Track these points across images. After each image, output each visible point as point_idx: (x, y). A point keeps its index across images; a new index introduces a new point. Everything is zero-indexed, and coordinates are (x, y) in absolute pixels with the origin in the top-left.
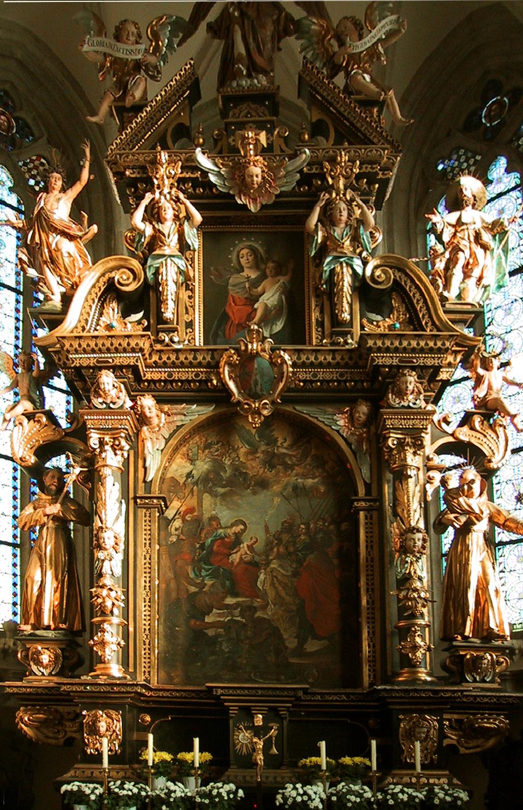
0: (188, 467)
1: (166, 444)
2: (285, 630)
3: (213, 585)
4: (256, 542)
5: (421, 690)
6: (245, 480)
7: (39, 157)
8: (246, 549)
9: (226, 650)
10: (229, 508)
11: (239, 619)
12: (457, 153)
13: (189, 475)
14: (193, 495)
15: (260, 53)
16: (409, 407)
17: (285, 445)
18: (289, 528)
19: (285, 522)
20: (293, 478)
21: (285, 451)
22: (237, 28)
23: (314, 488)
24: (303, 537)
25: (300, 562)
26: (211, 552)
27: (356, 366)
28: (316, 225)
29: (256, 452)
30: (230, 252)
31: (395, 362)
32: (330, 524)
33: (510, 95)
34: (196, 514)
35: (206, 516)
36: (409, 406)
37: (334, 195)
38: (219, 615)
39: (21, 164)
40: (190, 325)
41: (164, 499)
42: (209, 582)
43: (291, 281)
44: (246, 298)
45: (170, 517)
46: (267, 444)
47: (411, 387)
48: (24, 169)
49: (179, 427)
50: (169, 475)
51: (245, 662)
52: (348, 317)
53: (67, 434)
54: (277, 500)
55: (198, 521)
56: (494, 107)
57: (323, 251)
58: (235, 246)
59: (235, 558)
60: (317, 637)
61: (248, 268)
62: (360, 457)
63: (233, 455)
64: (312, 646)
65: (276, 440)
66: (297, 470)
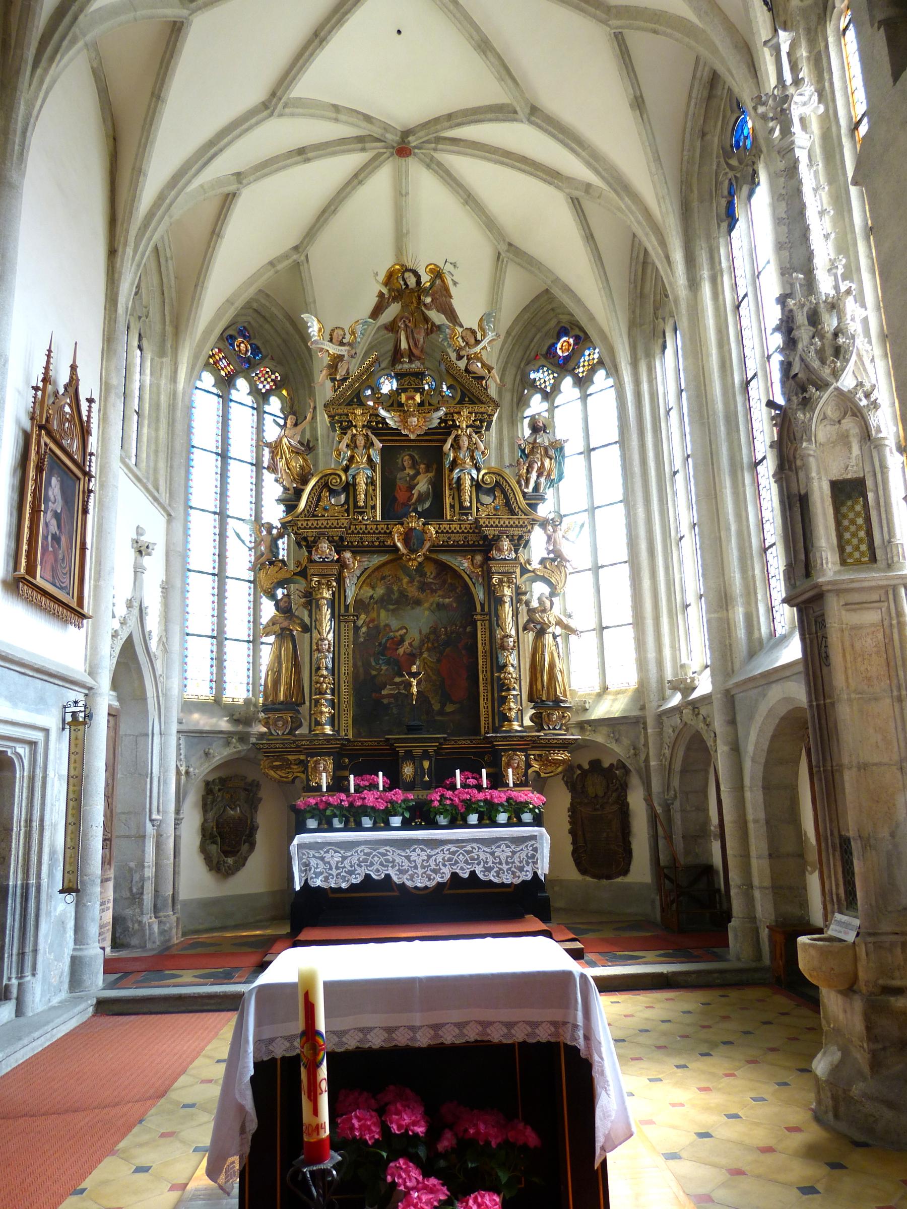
0: (371, 592)
7: (265, 367)
13: (372, 597)
16: (505, 559)
18: (434, 630)
20: (437, 598)
22: (403, 333)
26: (385, 648)
27: (474, 532)
31: (496, 533)
35: (382, 624)
38: (391, 689)
41: (357, 616)
42: (384, 668)
43: (435, 477)
47: (506, 548)
49: (366, 569)
50: (359, 598)
53: (295, 574)
54: (427, 613)
55: (377, 627)
57: (454, 464)
58: (400, 454)
59: (401, 651)
60: (452, 702)
64: (449, 708)
65: (426, 574)
66: (440, 593)
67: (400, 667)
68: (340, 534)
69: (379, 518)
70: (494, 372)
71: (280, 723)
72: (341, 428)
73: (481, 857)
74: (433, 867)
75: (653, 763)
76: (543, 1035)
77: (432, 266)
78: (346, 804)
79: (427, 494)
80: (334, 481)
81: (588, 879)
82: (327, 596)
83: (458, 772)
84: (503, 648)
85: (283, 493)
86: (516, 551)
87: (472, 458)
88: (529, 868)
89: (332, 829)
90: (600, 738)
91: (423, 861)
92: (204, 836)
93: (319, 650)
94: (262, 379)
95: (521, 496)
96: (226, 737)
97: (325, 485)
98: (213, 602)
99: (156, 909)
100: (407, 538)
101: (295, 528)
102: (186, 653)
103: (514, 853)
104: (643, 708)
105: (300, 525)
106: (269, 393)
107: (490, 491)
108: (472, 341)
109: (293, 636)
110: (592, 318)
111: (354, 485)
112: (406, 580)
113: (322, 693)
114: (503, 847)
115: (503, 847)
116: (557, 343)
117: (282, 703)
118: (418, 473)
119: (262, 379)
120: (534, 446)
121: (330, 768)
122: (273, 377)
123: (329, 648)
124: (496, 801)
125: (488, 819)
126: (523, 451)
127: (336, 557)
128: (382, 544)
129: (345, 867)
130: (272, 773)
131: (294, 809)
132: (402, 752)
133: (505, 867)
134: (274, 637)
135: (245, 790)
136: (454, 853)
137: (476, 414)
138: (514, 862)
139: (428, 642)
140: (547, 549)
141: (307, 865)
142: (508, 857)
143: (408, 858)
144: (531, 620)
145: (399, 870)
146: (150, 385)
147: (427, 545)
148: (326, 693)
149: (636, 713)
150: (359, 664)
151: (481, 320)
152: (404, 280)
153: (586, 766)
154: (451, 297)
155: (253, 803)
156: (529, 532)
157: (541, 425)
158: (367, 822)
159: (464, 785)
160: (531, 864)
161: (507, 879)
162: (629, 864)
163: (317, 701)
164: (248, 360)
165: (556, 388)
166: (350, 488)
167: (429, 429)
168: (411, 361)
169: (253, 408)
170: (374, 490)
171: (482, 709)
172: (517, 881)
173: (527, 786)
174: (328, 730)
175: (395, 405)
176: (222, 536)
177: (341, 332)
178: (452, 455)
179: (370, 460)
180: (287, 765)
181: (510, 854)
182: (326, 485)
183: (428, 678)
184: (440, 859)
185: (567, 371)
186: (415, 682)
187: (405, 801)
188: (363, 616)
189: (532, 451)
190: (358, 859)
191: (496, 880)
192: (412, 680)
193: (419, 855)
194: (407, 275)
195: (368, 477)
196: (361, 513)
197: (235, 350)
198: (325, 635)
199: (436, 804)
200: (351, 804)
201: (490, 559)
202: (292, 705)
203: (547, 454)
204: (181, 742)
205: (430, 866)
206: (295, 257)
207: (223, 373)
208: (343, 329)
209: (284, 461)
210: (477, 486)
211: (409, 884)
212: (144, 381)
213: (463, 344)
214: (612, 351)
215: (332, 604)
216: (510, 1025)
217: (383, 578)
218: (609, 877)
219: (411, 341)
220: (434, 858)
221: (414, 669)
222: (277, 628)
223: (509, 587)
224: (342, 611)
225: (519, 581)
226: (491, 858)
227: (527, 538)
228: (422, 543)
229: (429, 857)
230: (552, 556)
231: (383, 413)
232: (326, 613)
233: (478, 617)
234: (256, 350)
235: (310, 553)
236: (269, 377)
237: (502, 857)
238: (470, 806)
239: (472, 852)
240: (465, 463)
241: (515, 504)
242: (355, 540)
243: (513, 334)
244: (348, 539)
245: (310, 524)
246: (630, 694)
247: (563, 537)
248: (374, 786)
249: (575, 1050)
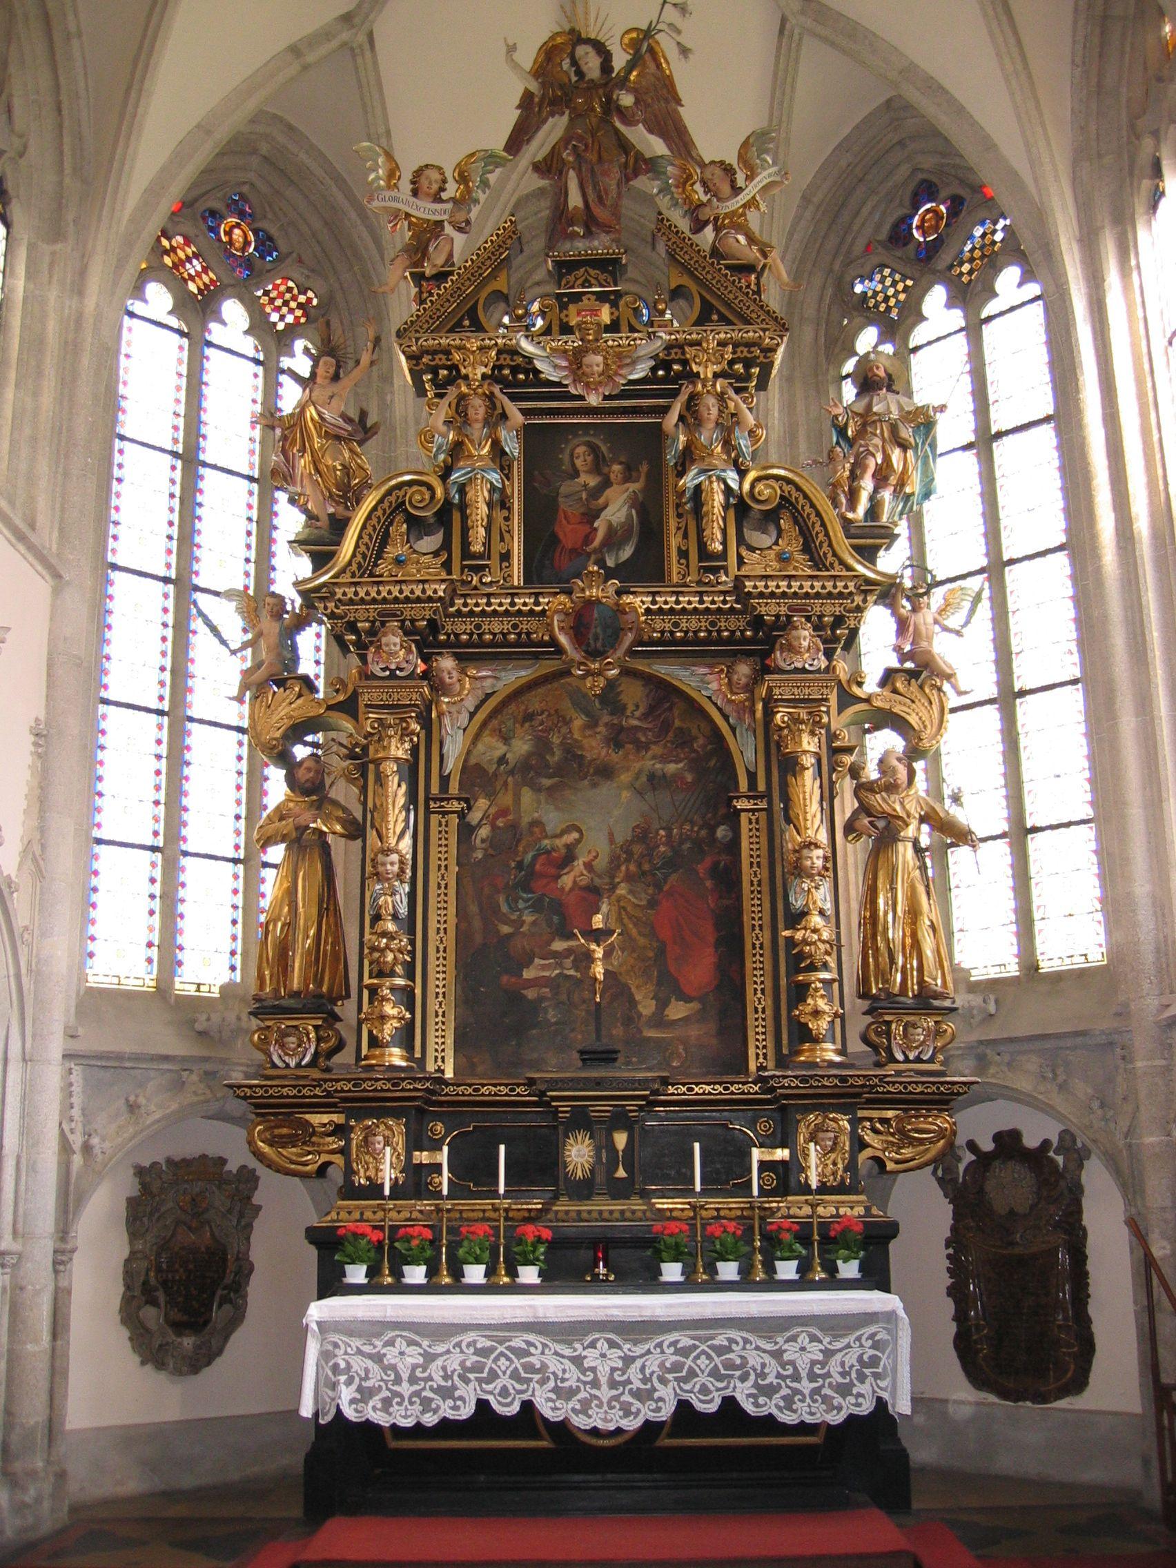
0: (500, 750)
1: (470, 720)
2: (638, 987)
3: (534, 923)
4: (596, 857)
5: (823, 1077)
6: (580, 765)
7: (285, 279)
8: (582, 867)
9: (553, 1020)
10: (557, 809)
11: (572, 972)
12: (881, 272)
13: (502, 760)
14: (507, 790)
15: (600, 200)
16: (804, 671)
17: (637, 714)
18: (642, 835)
19: (637, 826)
20: (648, 763)
21: (635, 723)
23: (677, 776)
24: (662, 849)
25: (658, 886)
26: (531, 874)
28: (676, 425)
29: (596, 725)
30: (562, 451)
31: (783, 610)
32: (701, 828)
33: (949, 202)
34: (510, 817)
35: (525, 820)
36: (804, 667)
37: (700, 387)
38: (544, 967)
39: (260, 293)
40: (506, 557)
41: (467, 801)
42: (528, 918)
43: (645, 490)
44: (583, 514)
45: (474, 823)
46: (612, 714)
48: (265, 300)
50: (473, 761)
51: (580, 1037)
52: (720, 548)
53: (330, 708)
54: (626, 794)
55: (514, 827)
56: (928, 217)
57: (687, 458)
58: (567, 442)
59: (567, 881)
61: (586, 472)
62: (742, 734)
63: (564, 730)
64: (677, 1010)
65: (624, 708)
66: (656, 750)
68: (428, 614)
69: (517, 578)
70: (775, 255)
73: (751, 1362)
74: (637, 1384)
77: (634, 35)
79: (627, 528)
80: (417, 496)
82: (400, 754)
84: (799, 871)
85: (306, 526)
86: (829, 654)
87: (727, 444)
88: (865, 1388)
91: (613, 1370)
94: (279, 302)
95: (839, 528)
98: (158, 773)
100: (579, 623)
101: (331, 605)
102: (95, 882)
103: (828, 1353)
105: (339, 596)
106: (292, 331)
107: (771, 517)
110: (989, 145)
111: (463, 507)
112: (579, 722)
114: (803, 1339)
115: (803, 1339)
116: (912, 217)
117: (296, 994)
118: (606, 483)
119: (279, 302)
120: (867, 420)
122: (302, 299)
123: (402, 871)
126: (842, 432)
127: (421, 667)
128: (526, 641)
129: (430, 1378)
132: (564, 1108)
133: (806, 1386)
134: (282, 846)
136: (685, 1352)
137: (735, 346)
138: (828, 1375)
139: (628, 860)
140: (898, 649)
142: (813, 1363)
144: (864, 809)
145: (555, 1389)
146: (25, 299)
148: (392, 974)
151: (746, 145)
152: (574, 62)
153: (987, 1145)
154: (679, 102)
156: (859, 609)
157: (881, 373)
160: (870, 1380)
161: (806, 1412)
163: (374, 991)
164: (248, 263)
165: (912, 313)
167: (631, 382)
168: (589, 234)
169: (257, 362)
170: (507, 519)
172: (836, 1418)
173: (857, 1193)
174: (396, 1056)
175: (555, 328)
177: (435, 175)
178: (682, 438)
179: (498, 451)
181: (820, 1357)
184: (653, 1365)
185: (934, 272)
186: (599, 953)
188: (482, 803)
189: (862, 432)
190: (462, 1364)
191: (787, 1418)
192: (593, 946)
193: (603, 1356)
194: (581, 50)
195: (493, 489)
197: (220, 240)
198: (392, 841)
204: (73, 1078)
205: (629, 1382)
206: (345, 36)
207: (192, 287)
208: (439, 169)
209: (308, 457)
210: (740, 507)
211: (580, 1422)
212: (12, 290)
213: (704, 199)
214: (1040, 217)
215: (410, 772)
217: (529, 717)
219: (590, 191)
220: (639, 1363)
221: (598, 921)
223: (812, 733)
224: (435, 789)
225: (838, 722)
226: (773, 1368)
227: (852, 624)
228: (615, 634)
229: (628, 1360)
230: (909, 665)
232: (397, 792)
233: (739, 805)
234: (266, 243)
235: (363, 658)
236: (294, 298)
237: (799, 1363)
239: (729, 1350)
240: (711, 455)
241: (825, 548)
242: (463, 628)
243: (816, 200)
244: (449, 628)
245: (362, 594)
247: (936, 622)
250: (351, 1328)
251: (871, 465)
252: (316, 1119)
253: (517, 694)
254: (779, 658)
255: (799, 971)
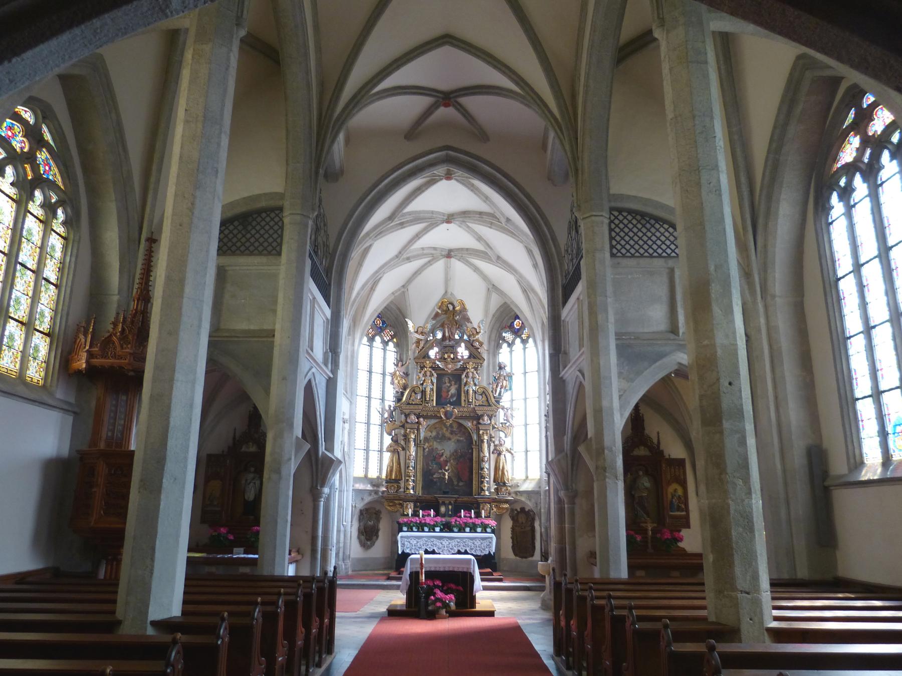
18: (456, 451)
20: (457, 438)
23: (462, 441)
40: (433, 400)
42: (435, 466)
54: (453, 443)
55: (432, 449)
57: (466, 384)
59: (442, 459)
60: (462, 481)
64: (461, 484)
67: (441, 466)
69: (435, 405)
71: (393, 488)
72: (421, 367)
75: (542, 510)
76: (465, 570)
78: (418, 522)
81: (518, 558)
83: (462, 511)
86: (490, 420)
88: (487, 549)
89: (412, 531)
90: (523, 499)
92: (359, 532)
93: (409, 459)
96: (370, 492)
97: (413, 391)
99: (344, 560)
100: (446, 414)
104: (540, 487)
108: (475, 333)
109: (398, 452)
111: (425, 391)
113: (410, 477)
118: (451, 385)
121: (412, 507)
124: (476, 523)
125: (473, 530)
127: (417, 420)
130: (389, 508)
131: (399, 523)
132: (441, 502)
133: (478, 548)
135: (375, 513)
136: (459, 542)
141: (404, 544)
143: (441, 543)
144: (495, 449)
147: (454, 417)
149: (538, 489)
150: (425, 464)
153: (519, 510)
155: (378, 519)
158: (426, 529)
159: (465, 516)
162: (534, 552)
163: (408, 480)
165: (513, 342)
166: (423, 393)
168: (450, 341)
171: (474, 485)
172: (482, 554)
176: (369, 406)
180: (395, 505)
182: (414, 391)
183: (452, 471)
186: (447, 474)
187: (441, 521)
188: (427, 444)
196: (427, 403)
199: (453, 523)
200: (420, 522)
201: (479, 423)
202: (397, 481)
203: (505, 379)
216: (458, 568)
217: (436, 428)
218: (526, 558)
222: (392, 449)
229: (449, 543)
231: (438, 363)
232: (412, 444)
234: (384, 323)
238: (466, 525)
246: (536, 481)
248: (429, 515)
249: (470, 573)
250: (408, 537)
251: (500, 385)
252: (396, 502)
253: (434, 424)
254: (481, 421)
255: (482, 478)
